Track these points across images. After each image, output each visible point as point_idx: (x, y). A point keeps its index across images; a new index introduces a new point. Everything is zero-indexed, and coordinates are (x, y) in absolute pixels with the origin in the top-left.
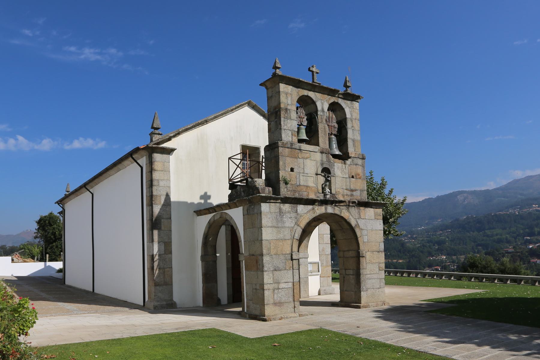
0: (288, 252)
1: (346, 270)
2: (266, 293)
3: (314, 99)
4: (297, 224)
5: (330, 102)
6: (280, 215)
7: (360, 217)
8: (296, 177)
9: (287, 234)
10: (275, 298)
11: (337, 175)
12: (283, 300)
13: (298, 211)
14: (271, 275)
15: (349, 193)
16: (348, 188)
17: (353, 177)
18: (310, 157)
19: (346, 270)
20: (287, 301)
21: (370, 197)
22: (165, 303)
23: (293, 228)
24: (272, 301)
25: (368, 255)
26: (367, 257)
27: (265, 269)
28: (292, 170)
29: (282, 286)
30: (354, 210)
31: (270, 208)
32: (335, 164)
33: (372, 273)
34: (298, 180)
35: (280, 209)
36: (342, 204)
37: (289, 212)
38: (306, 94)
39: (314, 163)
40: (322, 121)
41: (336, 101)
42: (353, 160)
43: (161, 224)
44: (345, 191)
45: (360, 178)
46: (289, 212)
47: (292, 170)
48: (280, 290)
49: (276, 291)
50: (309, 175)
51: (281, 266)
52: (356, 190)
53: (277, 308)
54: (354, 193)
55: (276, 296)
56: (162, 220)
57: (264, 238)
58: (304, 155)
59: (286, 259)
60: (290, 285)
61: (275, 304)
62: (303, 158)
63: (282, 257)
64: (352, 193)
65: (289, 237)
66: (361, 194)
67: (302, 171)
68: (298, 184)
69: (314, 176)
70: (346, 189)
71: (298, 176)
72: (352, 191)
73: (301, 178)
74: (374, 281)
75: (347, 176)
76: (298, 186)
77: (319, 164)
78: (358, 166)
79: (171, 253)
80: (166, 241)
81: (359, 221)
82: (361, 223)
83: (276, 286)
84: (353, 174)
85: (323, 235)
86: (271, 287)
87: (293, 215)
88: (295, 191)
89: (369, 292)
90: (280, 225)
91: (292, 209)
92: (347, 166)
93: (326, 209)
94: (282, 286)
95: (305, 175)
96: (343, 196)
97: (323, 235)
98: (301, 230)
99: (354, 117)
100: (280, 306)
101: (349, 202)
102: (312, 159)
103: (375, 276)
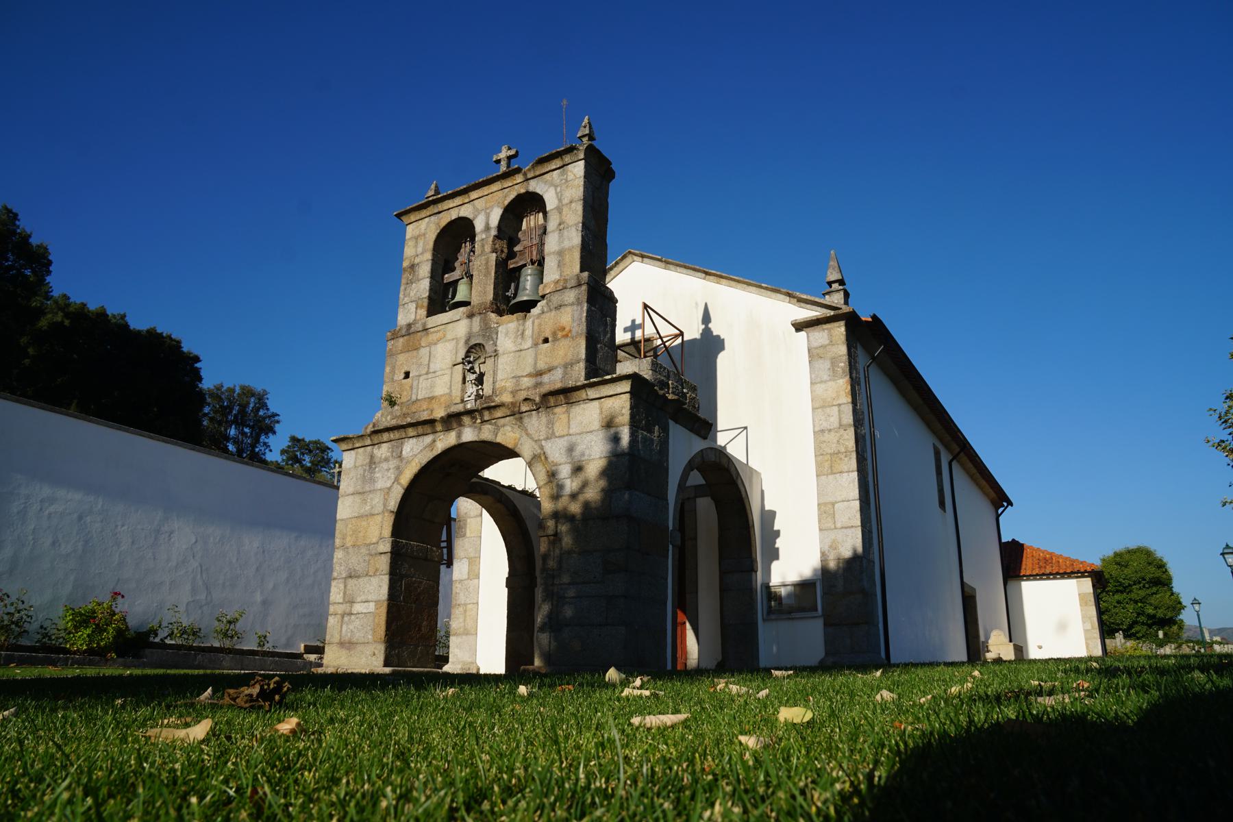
2: (332, 621)
4: (397, 480)
7: (553, 433)
8: (411, 387)
9: (376, 501)
12: (358, 636)
17: (546, 341)
20: (362, 640)
21: (843, 450)
24: (336, 639)
27: (335, 574)
28: (407, 375)
29: (358, 608)
35: (372, 457)
36: (499, 413)
40: (483, 251)
41: (523, 191)
45: (566, 336)
46: (386, 460)
47: (407, 375)
49: (346, 619)
51: (360, 568)
53: (344, 652)
54: (546, 378)
57: (338, 517)
58: (433, 337)
60: (371, 607)
61: (342, 644)
63: (364, 550)
64: (539, 379)
68: (414, 398)
71: (415, 384)
72: (540, 374)
78: (562, 310)
84: (548, 334)
85: (833, 504)
86: (340, 609)
87: (393, 464)
88: (405, 415)
93: (459, 436)
94: (358, 608)
96: (514, 393)
97: (833, 504)
98: (402, 491)
99: (566, 201)
100: (349, 649)
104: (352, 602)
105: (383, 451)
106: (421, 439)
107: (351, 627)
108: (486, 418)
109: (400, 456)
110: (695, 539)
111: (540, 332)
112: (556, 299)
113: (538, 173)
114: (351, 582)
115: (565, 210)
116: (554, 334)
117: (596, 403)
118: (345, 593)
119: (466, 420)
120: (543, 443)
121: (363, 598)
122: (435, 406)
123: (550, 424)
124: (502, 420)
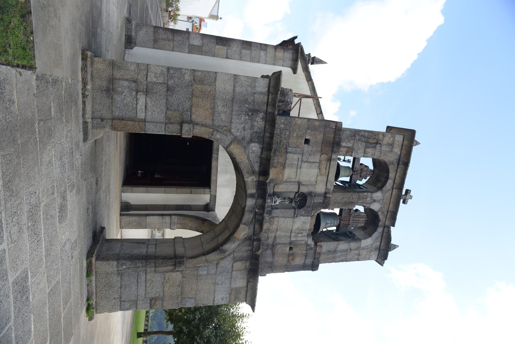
0: (194, 117)
1: (156, 244)
3: (384, 189)
5: (380, 214)
6: (251, 110)
8: (297, 147)
9: (222, 118)
10: (122, 82)
11: (296, 220)
13: (253, 144)
14: (161, 80)
15: (270, 241)
16: (278, 241)
17: (291, 249)
18: (321, 175)
19: (156, 244)
22: (133, 34)
23: (230, 131)
25: (176, 276)
26: (174, 275)
28: (307, 141)
29: (142, 99)
30: (244, 251)
31: (261, 93)
32: (309, 218)
33: (148, 285)
34: (294, 149)
37: (252, 126)
38: (391, 175)
39: (313, 179)
41: (380, 223)
42: (311, 249)
43: (221, 45)
44: (273, 235)
46: (252, 126)
47: (307, 141)
48: (134, 93)
50: (299, 170)
52: (273, 254)
54: (269, 252)
55: (126, 83)
56: (225, 48)
58: (324, 163)
59: (182, 113)
60: (141, 115)
62: (320, 162)
63: (187, 105)
65: (217, 123)
66: (267, 262)
67: (305, 159)
68: (290, 149)
69: (297, 180)
70: (275, 237)
73: (296, 157)
74: (134, 288)
75: (293, 239)
76: (286, 149)
77: (311, 189)
78: (304, 258)
79: (190, 52)
80: (204, 49)
81: (229, 259)
82: (226, 263)
83: (143, 87)
84: (294, 250)
87: (247, 134)
89: (116, 279)
90: (236, 108)
91: (256, 132)
92: (306, 239)
93: (252, 196)
94: (142, 99)
95: (300, 163)
99: (361, 251)
101: (259, 240)
102: (319, 178)
103: (142, 292)
104: (147, 92)
105: (259, 123)
107: (126, 92)
108: (257, 216)
109: (251, 141)
110: (191, 193)
111: (296, 245)
112: (311, 252)
113: (384, 234)
114: (163, 89)
115: (356, 252)
116: (293, 254)
117: (245, 285)
118: (155, 83)
119: (260, 201)
120: (232, 255)
121: (149, 104)
122: (278, 169)
123: (241, 259)
124: (252, 227)
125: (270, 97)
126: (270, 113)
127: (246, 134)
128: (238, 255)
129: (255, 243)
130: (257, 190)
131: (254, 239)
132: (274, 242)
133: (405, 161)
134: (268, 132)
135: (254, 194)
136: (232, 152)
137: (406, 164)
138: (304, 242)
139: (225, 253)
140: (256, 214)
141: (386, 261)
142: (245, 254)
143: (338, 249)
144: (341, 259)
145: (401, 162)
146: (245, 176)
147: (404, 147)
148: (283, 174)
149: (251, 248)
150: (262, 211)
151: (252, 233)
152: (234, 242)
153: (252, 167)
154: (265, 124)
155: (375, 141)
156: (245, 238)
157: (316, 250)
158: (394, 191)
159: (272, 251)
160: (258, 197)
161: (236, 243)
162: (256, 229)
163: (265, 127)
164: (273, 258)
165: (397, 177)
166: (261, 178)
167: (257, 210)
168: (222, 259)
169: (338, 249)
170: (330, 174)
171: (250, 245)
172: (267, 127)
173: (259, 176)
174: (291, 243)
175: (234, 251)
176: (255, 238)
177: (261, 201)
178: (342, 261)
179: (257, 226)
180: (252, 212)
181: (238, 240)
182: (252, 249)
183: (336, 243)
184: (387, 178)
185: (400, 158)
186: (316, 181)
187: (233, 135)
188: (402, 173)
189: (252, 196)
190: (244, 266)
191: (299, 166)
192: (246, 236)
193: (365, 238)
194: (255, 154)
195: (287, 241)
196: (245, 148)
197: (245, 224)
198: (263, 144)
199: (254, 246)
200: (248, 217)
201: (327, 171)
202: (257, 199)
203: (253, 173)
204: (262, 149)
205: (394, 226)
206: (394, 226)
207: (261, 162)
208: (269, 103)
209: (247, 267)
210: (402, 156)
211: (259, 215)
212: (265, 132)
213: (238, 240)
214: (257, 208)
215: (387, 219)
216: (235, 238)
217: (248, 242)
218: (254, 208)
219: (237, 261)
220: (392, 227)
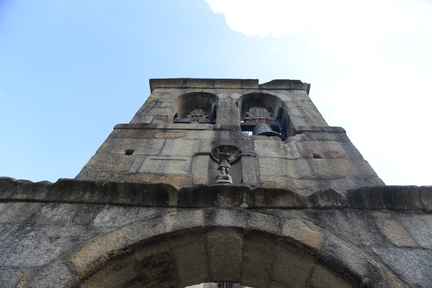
11: (261, 155)
17: (316, 156)
32: (256, 141)
58: (167, 134)
70: (302, 178)
75: (298, 155)
93: (210, 216)
101: (313, 198)
106: (134, 211)
108: (258, 204)
119: (223, 200)
124: (285, 213)
125: (19, 197)
126: (49, 194)
127: (67, 234)
128: (368, 239)
129: (322, 203)
130: (198, 208)
131: (314, 208)
132: (311, 179)
133: (182, 83)
134: (82, 196)
135: (206, 213)
136: (93, 259)
137: (185, 81)
138: (300, 144)
139: (376, 269)
140: (253, 208)
141: (303, 82)
142: (359, 223)
143: (301, 115)
144: (312, 111)
145: (184, 86)
146: (162, 231)
147: (167, 86)
148: (175, 175)
149: (337, 212)
150: (245, 195)
151: (300, 212)
152: (334, 246)
153: (145, 219)
154: (65, 202)
155: (154, 103)
156: (316, 224)
157: (308, 131)
158: (216, 86)
159: (330, 179)
160: (213, 205)
161: (336, 242)
162: (288, 205)
163: (71, 202)
164: (344, 177)
165: (200, 87)
166: (173, 202)
167: (245, 205)
168: (399, 276)
169: (301, 115)
170: (186, 128)
171: (332, 214)
172: (72, 198)
173: (168, 206)
174: (306, 158)
175: (361, 246)
176: (309, 205)
177: (222, 198)
178: (317, 111)
179: (281, 203)
180: (249, 215)
181: (326, 238)
182: (339, 208)
183: (291, 118)
184: (202, 94)
185: (179, 88)
186: (195, 139)
187: (53, 261)
188: (195, 83)
189: (210, 216)
190: (392, 222)
191: (166, 158)
192: (311, 224)
193: (279, 99)
194: (119, 217)
195: (305, 162)
196: (97, 234)
197: (280, 226)
198: (104, 204)
199: (330, 204)
200: (261, 222)
201: (181, 131)
202: (219, 207)
203: (158, 217)
204: (112, 204)
205: (257, 81)
206: (257, 81)
207: (140, 206)
208: (30, 197)
209: (389, 215)
210: (176, 86)
211: (254, 200)
212: (80, 202)
213: (326, 238)
214: (239, 206)
215: (251, 88)
216: (323, 245)
217: (325, 218)
218: (241, 211)
219: (384, 237)
220: (260, 83)
